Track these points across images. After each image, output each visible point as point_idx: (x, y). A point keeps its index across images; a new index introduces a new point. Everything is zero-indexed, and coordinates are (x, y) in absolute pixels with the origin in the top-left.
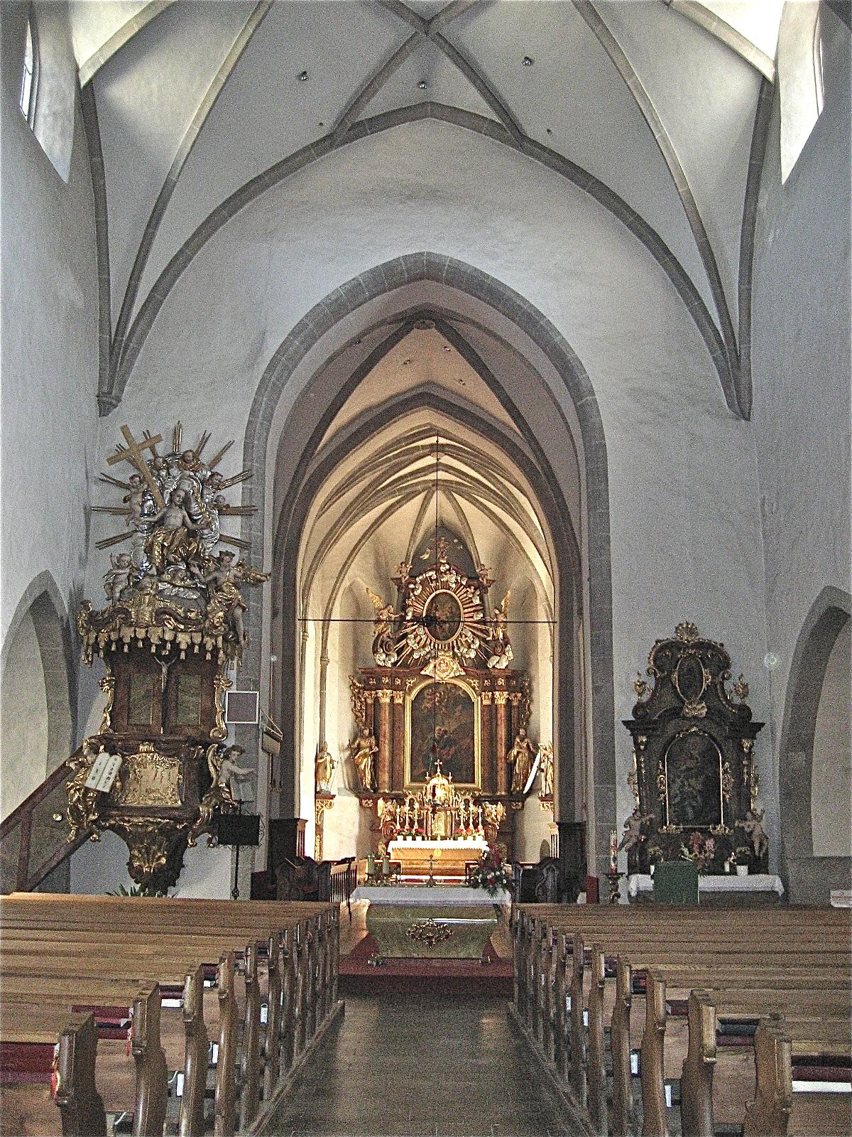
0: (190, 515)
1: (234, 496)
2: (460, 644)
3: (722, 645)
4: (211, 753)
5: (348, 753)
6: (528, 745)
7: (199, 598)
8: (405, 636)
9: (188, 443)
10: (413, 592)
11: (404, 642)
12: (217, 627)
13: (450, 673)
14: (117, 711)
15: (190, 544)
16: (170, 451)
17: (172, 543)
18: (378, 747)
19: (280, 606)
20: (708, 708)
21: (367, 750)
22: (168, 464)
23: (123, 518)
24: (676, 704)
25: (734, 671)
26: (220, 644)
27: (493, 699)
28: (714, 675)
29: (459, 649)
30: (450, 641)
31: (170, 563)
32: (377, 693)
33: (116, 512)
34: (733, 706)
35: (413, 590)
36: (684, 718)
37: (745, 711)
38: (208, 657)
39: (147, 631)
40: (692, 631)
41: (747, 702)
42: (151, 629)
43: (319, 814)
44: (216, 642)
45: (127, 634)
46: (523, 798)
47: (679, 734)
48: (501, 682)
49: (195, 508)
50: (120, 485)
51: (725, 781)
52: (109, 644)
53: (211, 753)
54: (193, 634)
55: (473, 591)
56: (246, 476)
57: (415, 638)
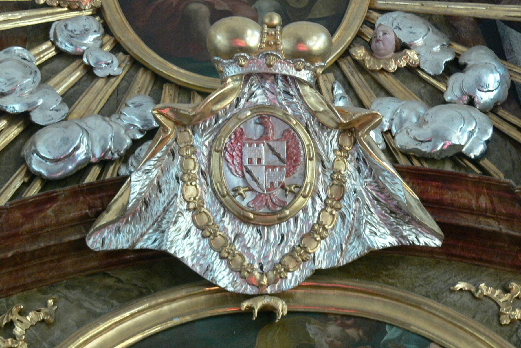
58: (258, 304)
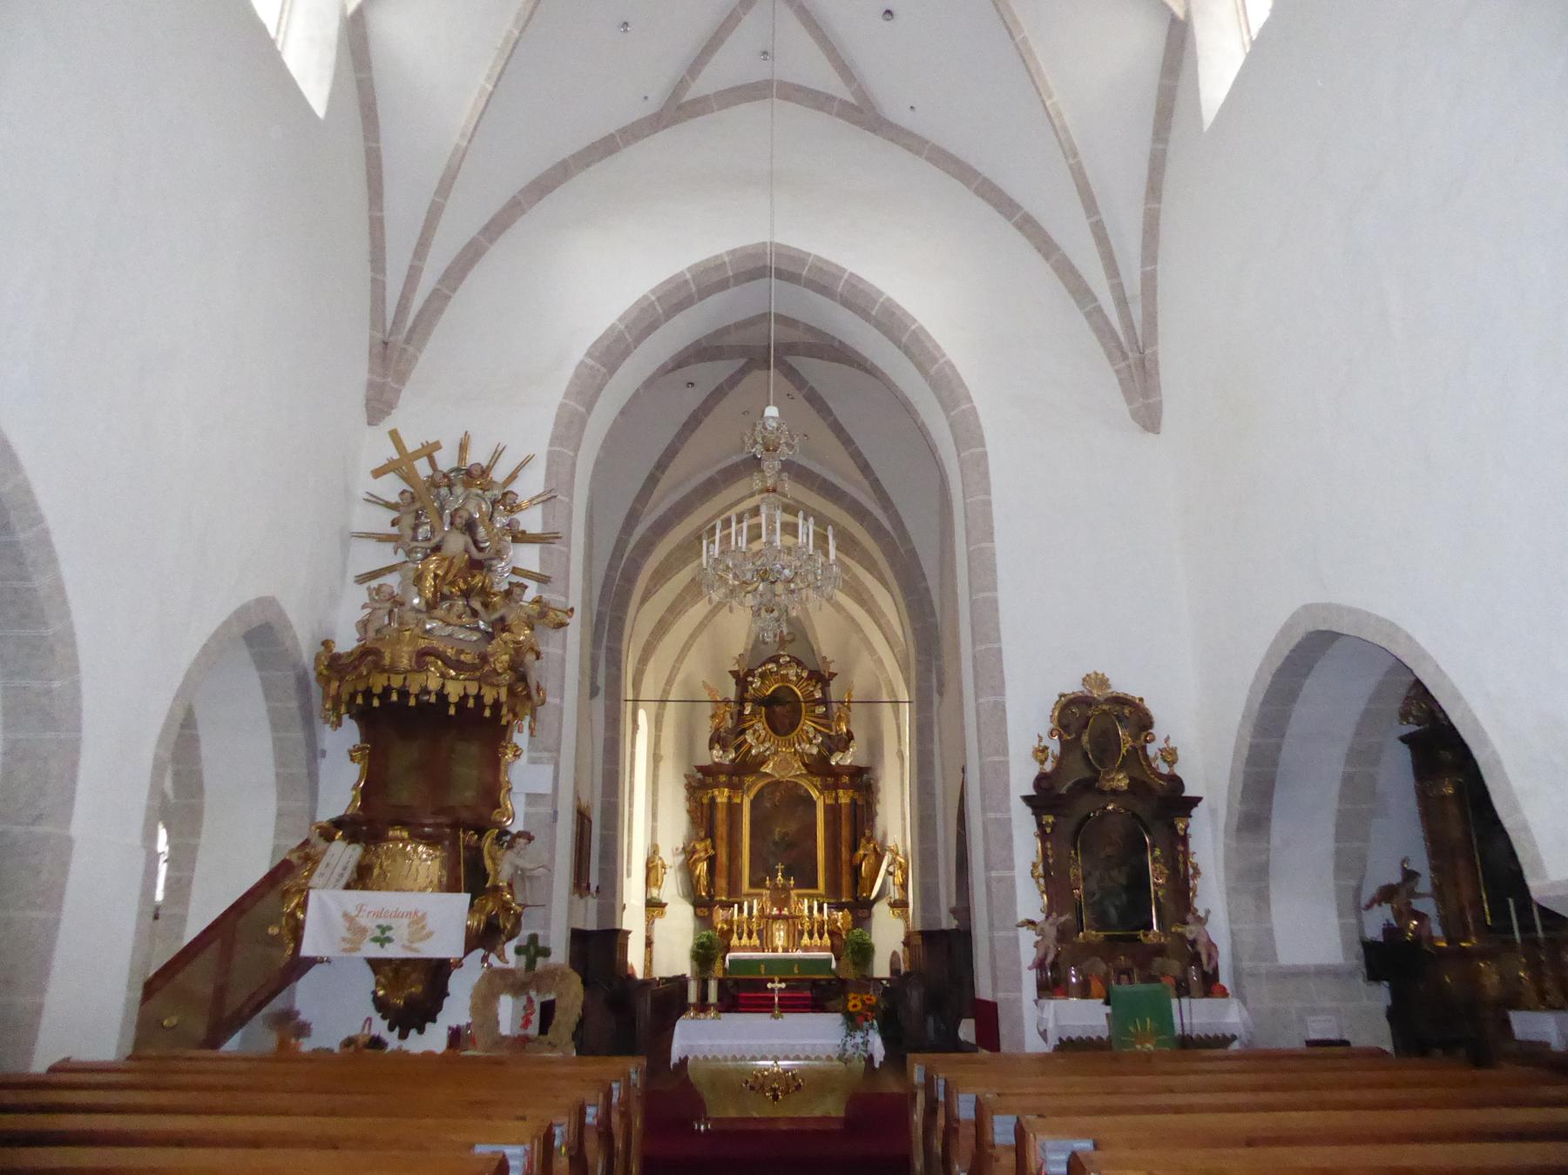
0: (476, 543)
1: (531, 521)
2: (801, 740)
3: (1141, 699)
4: (489, 840)
5: (681, 858)
6: (875, 848)
7: (478, 640)
8: (743, 732)
9: (478, 456)
10: (751, 685)
11: (741, 738)
12: (499, 674)
13: (790, 772)
14: (371, 789)
15: (473, 577)
16: (455, 465)
17: (446, 573)
19: (601, 681)
20: (1130, 778)
21: (702, 854)
22: (449, 480)
23: (389, 547)
24: (1087, 774)
25: (1159, 731)
26: (503, 698)
27: (837, 798)
28: (1135, 737)
29: (800, 745)
30: (790, 737)
31: (444, 597)
32: (713, 793)
33: (382, 538)
34: (1161, 776)
35: (752, 683)
36: (1102, 792)
37: (1176, 782)
38: (487, 713)
39: (405, 679)
40: (1103, 682)
41: (1179, 770)
42: (410, 677)
43: (650, 922)
44: (498, 693)
45: (378, 683)
46: (869, 904)
47: (1094, 812)
48: (846, 779)
49: (481, 532)
50: (388, 505)
51: (1157, 878)
52: (353, 696)
53: (489, 840)
54: (467, 682)
55: (814, 684)
56: (547, 499)
57: (754, 734)
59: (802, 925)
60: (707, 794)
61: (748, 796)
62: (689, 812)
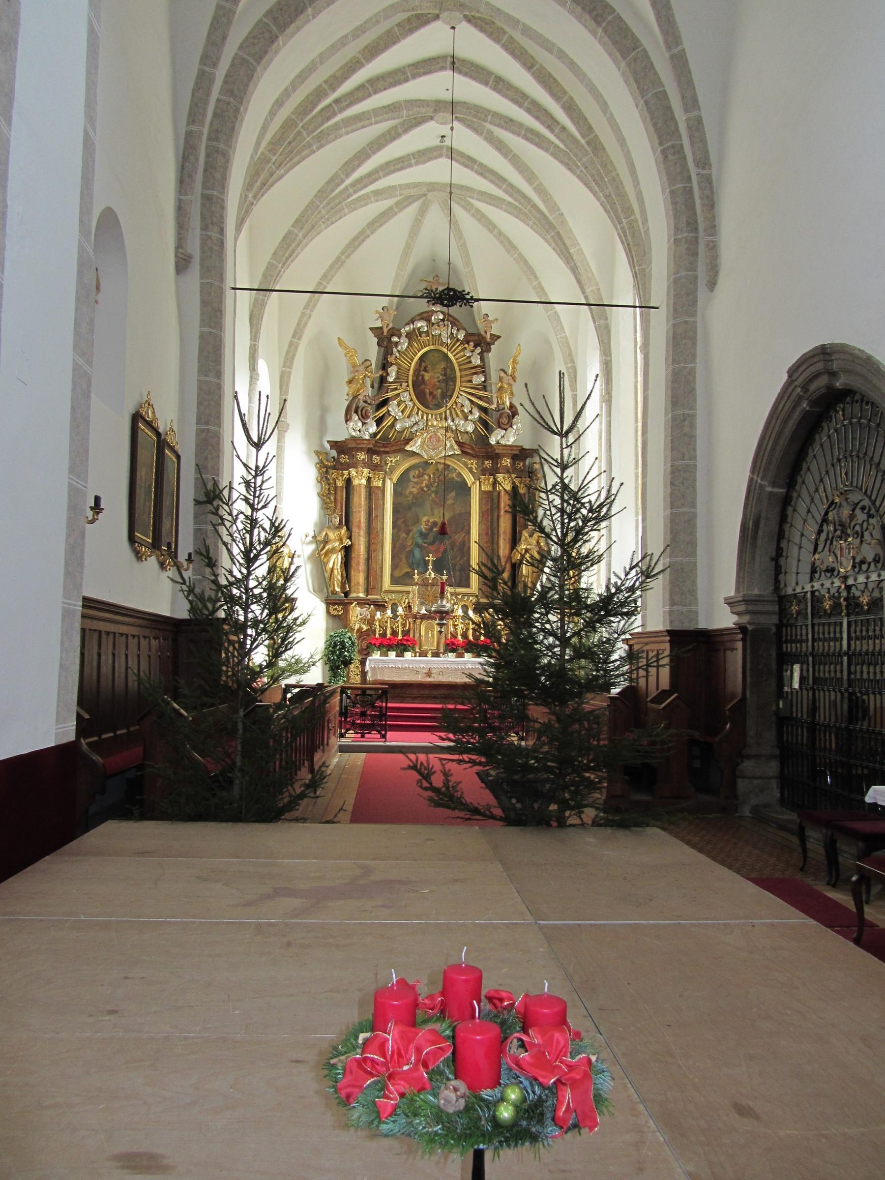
10: (396, 347)
18: (350, 538)
58: (430, 461)
59: (455, 626)
60: (343, 475)
61: (391, 479)
62: (321, 495)
